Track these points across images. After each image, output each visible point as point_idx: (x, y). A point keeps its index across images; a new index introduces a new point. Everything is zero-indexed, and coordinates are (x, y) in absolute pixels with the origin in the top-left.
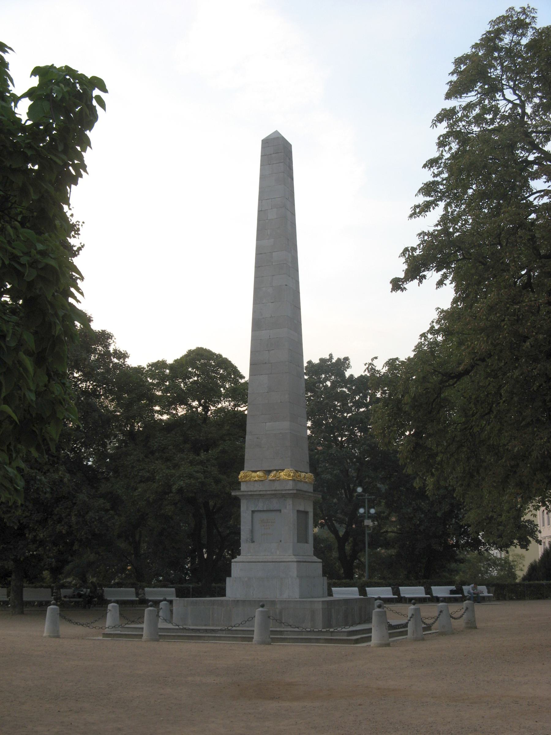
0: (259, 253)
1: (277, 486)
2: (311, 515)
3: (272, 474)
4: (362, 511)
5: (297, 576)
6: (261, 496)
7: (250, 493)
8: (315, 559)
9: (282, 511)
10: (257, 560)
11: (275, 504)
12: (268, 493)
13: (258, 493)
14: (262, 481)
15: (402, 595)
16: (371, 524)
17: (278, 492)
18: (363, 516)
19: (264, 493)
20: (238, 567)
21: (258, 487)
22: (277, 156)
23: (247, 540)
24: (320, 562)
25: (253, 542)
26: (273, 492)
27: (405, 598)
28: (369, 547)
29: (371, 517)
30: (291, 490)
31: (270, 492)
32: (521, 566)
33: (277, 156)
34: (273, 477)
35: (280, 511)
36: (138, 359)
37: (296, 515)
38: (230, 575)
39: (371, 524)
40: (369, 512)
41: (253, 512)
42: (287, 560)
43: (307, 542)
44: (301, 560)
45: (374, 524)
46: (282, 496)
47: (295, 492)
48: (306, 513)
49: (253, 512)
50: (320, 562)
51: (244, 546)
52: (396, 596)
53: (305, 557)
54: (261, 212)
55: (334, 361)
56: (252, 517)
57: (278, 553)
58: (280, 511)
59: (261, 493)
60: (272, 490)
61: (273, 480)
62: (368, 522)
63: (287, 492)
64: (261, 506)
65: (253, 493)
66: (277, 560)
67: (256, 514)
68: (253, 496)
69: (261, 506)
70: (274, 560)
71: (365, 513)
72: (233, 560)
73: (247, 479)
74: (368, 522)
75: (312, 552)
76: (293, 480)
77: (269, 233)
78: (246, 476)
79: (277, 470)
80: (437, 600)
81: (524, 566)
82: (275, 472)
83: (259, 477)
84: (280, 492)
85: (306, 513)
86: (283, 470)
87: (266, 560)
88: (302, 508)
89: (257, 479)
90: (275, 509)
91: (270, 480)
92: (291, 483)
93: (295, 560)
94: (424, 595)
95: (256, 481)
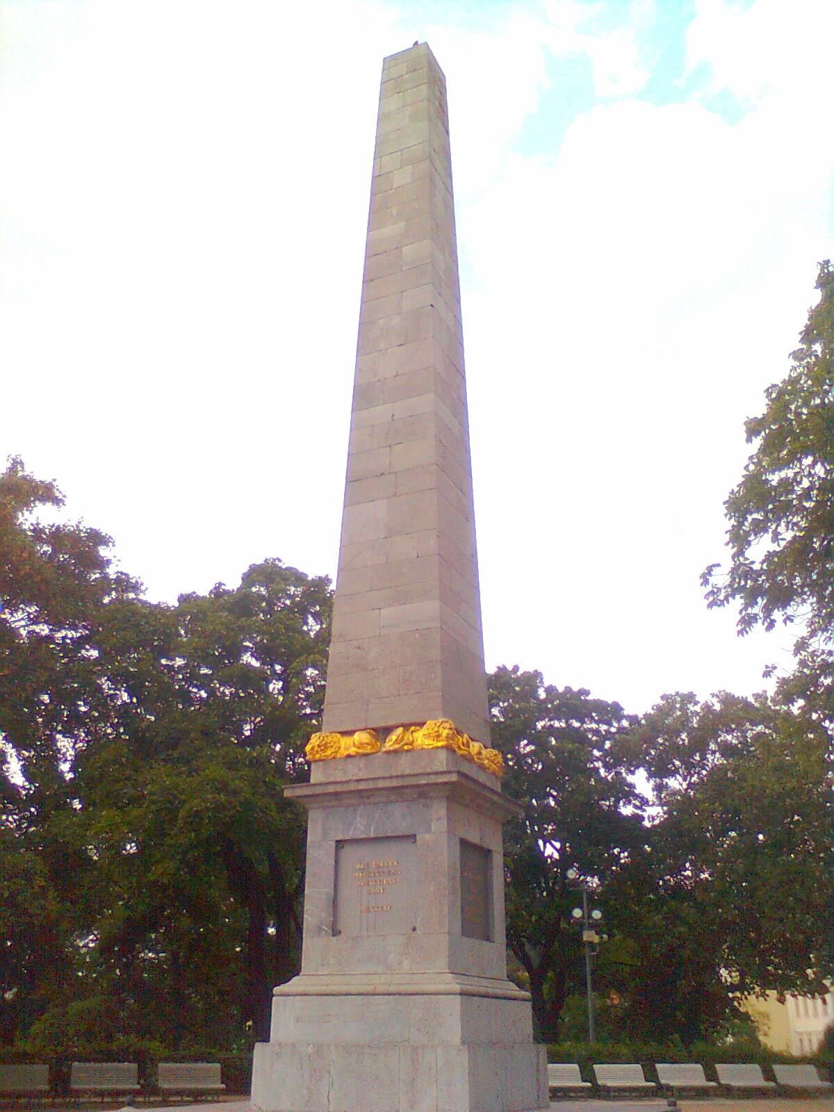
0: (373, 253)
1: (404, 765)
2: (498, 860)
3: (391, 743)
4: (577, 913)
5: (463, 1043)
6: (361, 796)
7: (331, 789)
8: (512, 989)
9: (418, 837)
10: (345, 989)
11: (399, 818)
12: (381, 784)
13: (352, 787)
14: (367, 755)
15: (663, 1081)
16: (596, 939)
17: (407, 782)
18: (580, 925)
19: (371, 785)
20: (288, 1009)
21: (354, 771)
22: (417, 88)
23: (321, 929)
24: (524, 1000)
25: (336, 932)
26: (395, 783)
27: (669, 1088)
28: (594, 989)
29: (595, 926)
30: (442, 773)
31: (387, 784)
32: (766, 1028)
33: (417, 88)
34: (396, 742)
35: (412, 838)
36: (161, 589)
37: (457, 853)
38: (266, 1039)
39: (596, 939)
40: (590, 917)
41: (340, 844)
42: (432, 988)
43: (488, 939)
44: (474, 989)
45: (602, 938)
46: (415, 792)
47: (454, 778)
48: (487, 853)
49: (340, 844)
50: (524, 1000)
51: (312, 947)
52: (589, 1084)
53: (485, 982)
54: (379, 179)
55: (519, 673)
56: (337, 862)
57: (406, 965)
58: (412, 838)
59: (362, 786)
60: (391, 777)
61: (396, 751)
62: (589, 936)
63: (433, 779)
64: (360, 825)
65: (339, 788)
66: (404, 988)
67: (347, 851)
68: (337, 797)
69: (360, 825)
70: (392, 989)
71: (583, 917)
72: (276, 990)
73: (329, 752)
74: (589, 936)
75: (501, 969)
76: (449, 748)
77: (394, 213)
78: (324, 747)
79: (406, 727)
80: (728, 1092)
81: (769, 1028)
82: (400, 730)
83: (361, 745)
84: (413, 781)
85: (487, 853)
86: (422, 724)
87: (370, 989)
88: (474, 838)
89: (353, 750)
90: (398, 833)
91: (388, 752)
92: (443, 756)
93: (457, 988)
94: (758, 1081)
95: (349, 756)
